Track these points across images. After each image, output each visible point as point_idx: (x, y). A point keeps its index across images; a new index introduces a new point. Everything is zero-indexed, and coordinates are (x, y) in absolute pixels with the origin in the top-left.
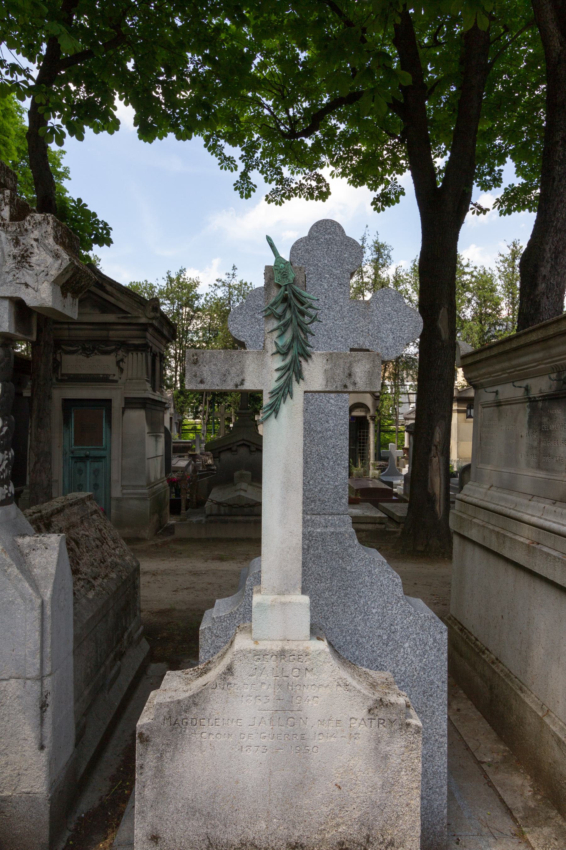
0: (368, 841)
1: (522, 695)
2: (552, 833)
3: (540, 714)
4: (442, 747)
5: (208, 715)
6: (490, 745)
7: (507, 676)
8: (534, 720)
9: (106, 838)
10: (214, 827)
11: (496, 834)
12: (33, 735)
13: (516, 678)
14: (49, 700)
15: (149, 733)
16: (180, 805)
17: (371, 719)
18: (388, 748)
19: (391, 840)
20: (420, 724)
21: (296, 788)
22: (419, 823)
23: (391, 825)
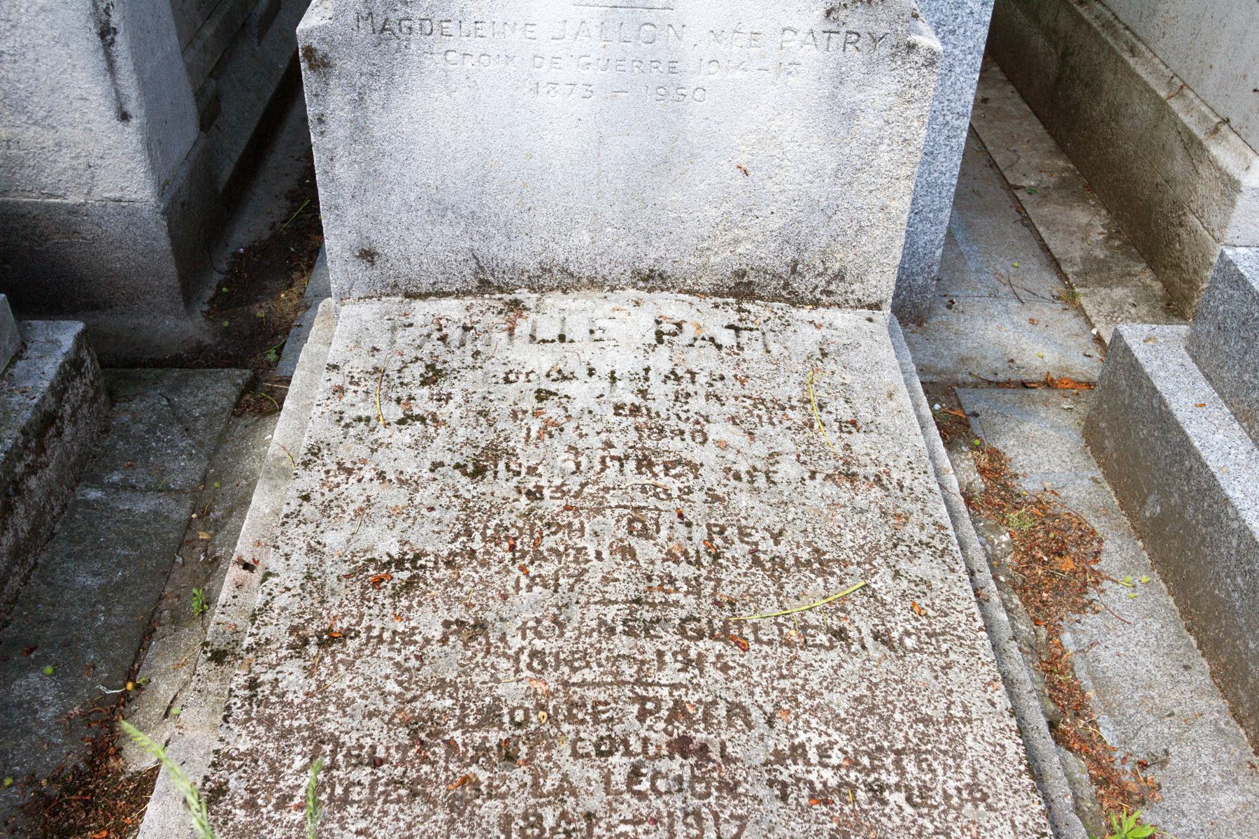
0: (794, 271)
1: (1131, 61)
3: (1163, 94)
4: (954, 137)
5: (458, 13)
6: (1038, 160)
7: (1108, 25)
8: (1145, 107)
9: (290, 286)
10: (486, 238)
12: (99, 90)
13: (1127, 28)
14: (115, 19)
15: (326, 48)
16: (413, 196)
17: (830, 32)
18: (861, 96)
19: (840, 270)
20: (938, 46)
21: (654, 170)
22: (900, 242)
23: (843, 245)
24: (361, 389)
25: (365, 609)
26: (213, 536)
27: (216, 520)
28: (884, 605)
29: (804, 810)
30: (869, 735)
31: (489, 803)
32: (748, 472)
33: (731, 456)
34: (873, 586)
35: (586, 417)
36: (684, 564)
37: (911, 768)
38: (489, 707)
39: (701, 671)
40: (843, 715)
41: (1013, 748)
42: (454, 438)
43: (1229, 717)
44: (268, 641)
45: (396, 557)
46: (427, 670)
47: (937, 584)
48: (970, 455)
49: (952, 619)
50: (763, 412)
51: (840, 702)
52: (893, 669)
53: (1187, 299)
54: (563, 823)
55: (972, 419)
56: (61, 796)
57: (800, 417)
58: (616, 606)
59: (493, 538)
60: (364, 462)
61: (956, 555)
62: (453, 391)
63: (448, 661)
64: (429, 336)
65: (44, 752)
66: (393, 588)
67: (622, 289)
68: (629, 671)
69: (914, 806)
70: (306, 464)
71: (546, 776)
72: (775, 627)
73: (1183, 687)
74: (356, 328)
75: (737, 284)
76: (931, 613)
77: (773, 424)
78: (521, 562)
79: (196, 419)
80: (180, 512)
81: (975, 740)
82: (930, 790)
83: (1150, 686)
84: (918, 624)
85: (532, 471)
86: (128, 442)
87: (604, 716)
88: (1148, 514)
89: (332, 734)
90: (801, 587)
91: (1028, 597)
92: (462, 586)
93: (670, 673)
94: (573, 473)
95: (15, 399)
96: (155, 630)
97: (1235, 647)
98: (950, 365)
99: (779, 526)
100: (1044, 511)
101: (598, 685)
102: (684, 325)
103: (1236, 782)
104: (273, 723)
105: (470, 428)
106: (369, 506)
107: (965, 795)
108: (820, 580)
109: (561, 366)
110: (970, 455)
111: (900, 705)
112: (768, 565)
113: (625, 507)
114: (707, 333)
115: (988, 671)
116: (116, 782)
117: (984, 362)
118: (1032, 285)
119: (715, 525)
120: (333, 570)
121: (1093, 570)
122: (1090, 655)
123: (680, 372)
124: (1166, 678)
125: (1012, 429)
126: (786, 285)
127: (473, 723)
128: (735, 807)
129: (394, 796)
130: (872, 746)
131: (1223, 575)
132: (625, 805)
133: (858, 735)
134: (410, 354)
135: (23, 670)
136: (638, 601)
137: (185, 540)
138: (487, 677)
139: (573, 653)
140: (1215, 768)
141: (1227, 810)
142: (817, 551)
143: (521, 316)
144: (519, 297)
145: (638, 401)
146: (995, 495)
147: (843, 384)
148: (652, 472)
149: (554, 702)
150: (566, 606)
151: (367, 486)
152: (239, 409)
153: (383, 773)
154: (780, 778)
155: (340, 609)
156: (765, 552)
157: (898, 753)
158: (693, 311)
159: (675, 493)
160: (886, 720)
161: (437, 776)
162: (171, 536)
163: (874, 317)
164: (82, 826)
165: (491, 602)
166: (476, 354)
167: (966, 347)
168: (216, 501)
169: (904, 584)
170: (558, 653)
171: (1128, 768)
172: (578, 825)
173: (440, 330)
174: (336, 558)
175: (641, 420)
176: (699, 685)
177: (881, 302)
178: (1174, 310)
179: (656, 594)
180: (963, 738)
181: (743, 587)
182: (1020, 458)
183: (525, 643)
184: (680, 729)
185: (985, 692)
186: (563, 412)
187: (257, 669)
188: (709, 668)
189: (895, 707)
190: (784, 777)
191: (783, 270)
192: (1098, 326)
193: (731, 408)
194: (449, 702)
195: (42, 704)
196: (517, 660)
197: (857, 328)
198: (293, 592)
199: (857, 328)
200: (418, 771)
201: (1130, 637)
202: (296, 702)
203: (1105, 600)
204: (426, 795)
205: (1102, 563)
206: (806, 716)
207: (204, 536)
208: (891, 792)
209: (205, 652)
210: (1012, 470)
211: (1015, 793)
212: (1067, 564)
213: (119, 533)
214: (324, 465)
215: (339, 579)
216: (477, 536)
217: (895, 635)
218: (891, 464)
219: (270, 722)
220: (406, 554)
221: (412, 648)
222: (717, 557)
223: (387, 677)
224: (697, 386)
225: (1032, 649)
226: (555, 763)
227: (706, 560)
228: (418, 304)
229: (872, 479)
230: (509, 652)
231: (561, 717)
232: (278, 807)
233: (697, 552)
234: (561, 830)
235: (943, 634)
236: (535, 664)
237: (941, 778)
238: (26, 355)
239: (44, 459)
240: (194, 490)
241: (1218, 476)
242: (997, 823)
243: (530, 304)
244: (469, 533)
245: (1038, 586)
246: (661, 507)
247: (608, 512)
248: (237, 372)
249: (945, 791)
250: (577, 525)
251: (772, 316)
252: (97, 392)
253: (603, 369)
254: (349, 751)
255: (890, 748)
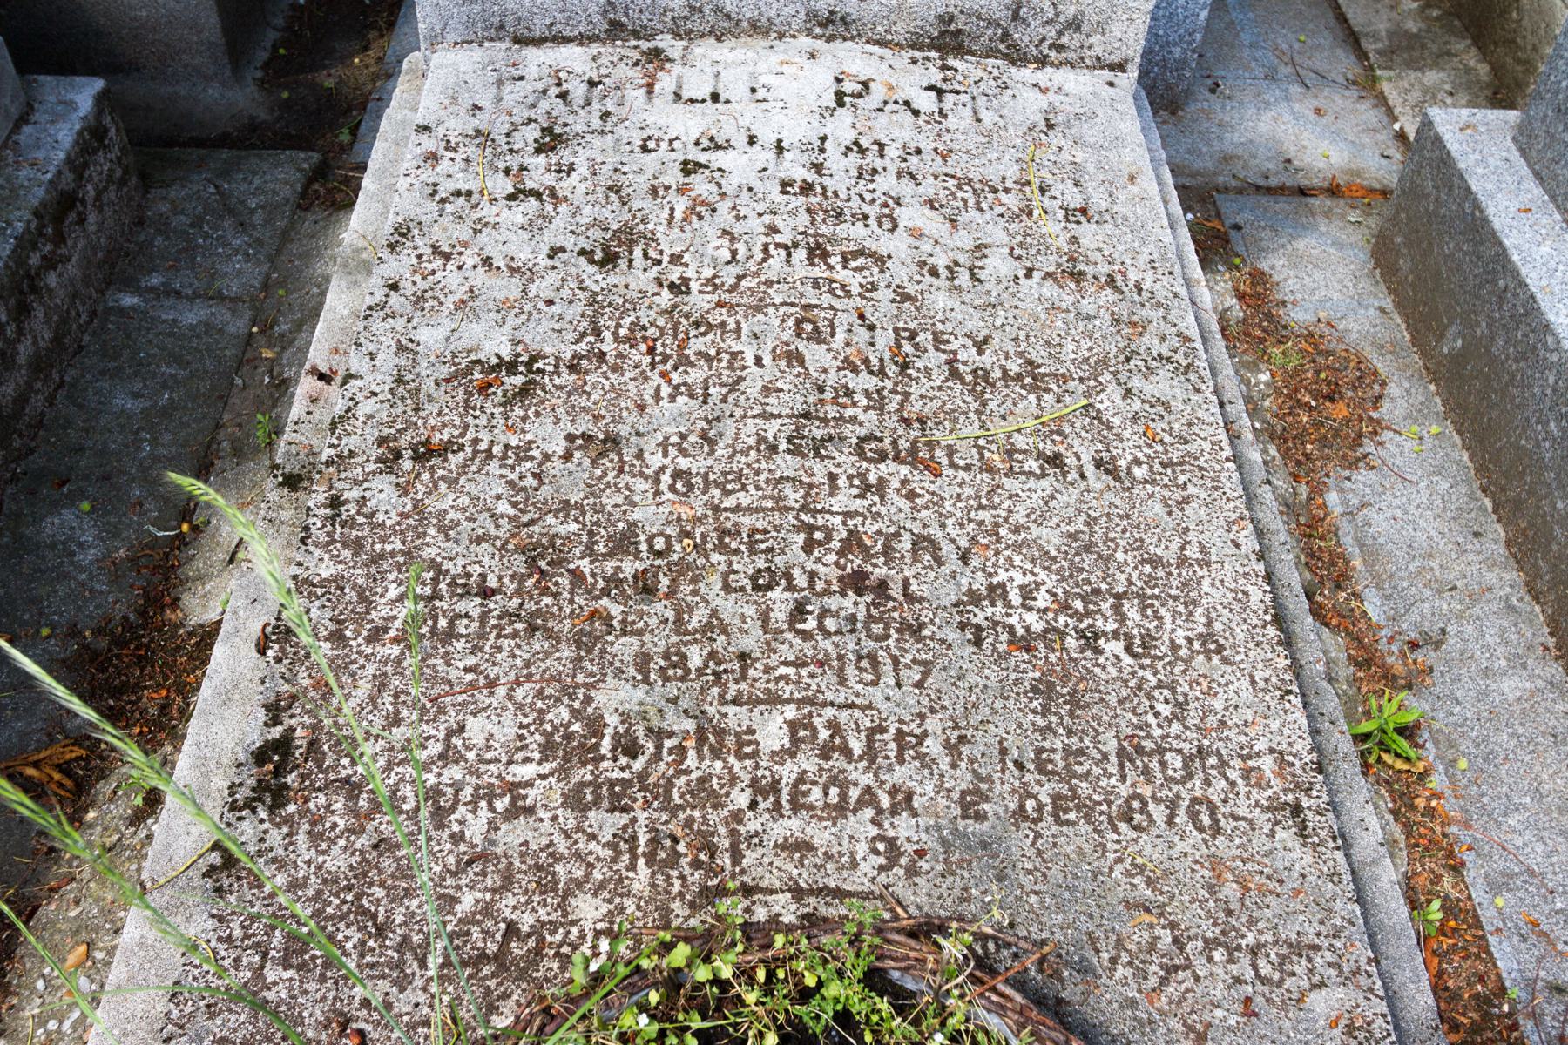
0: (1016, 16)
2: (1443, 82)
9: (366, 48)
11: (1310, 79)
19: (1075, 17)
24: (459, 157)
25: (469, 419)
26: (279, 354)
27: (283, 335)
28: (1110, 428)
29: (1002, 657)
30: (1084, 575)
31: (622, 640)
32: (948, 267)
33: (926, 247)
34: (1098, 405)
35: (745, 195)
36: (864, 374)
37: (1133, 613)
38: (623, 534)
39: (882, 498)
40: (1053, 553)
41: (1258, 595)
42: (578, 218)
43: (1523, 593)
44: (352, 454)
45: (507, 359)
46: (547, 490)
47: (1177, 405)
48: (1227, 276)
49: (1193, 448)
50: (969, 195)
51: (1050, 537)
52: (1118, 502)
53: (1520, 86)
54: (712, 664)
55: (1233, 233)
56: (110, 650)
57: (1016, 202)
58: (780, 421)
59: (627, 339)
60: (466, 245)
61: (1203, 373)
62: (576, 160)
63: (573, 479)
64: (545, 92)
65: (87, 600)
66: (504, 395)
67: (793, 36)
68: (793, 496)
69: (1135, 656)
70: (392, 247)
71: (691, 612)
72: (974, 451)
73: (1471, 557)
74: (451, 81)
75: (942, 33)
76: (1167, 439)
77: (981, 210)
78: (662, 367)
79: (253, 212)
80: (238, 325)
81: (1213, 585)
82: (1154, 639)
83: (1430, 555)
84: (1150, 452)
85: (676, 259)
86: (168, 238)
87: (762, 546)
88: (1445, 350)
89: (433, 561)
90: (1009, 404)
91: (1288, 449)
92: (589, 394)
93: (844, 499)
94: (728, 263)
95: (23, 173)
96: (212, 464)
97: (1539, 507)
98: (1209, 165)
99: (984, 333)
100: (1316, 346)
101: (756, 510)
102: (872, 85)
103: (1524, 666)
104: (361, 546)
105: (598, 207)
106: (472, 299)
107: (1196, 645)
108: (1032, 398)
109: (714, 132)
110: (1227, 276)
111: (1123, 543)
112: (969, 378)
113: (793, 305)
114: (901, 96)
115: (1232, 509)
116: (174, 636)
117: (1253, 162)
118: (1320, 63)
119: (905, 329)
120: (429, 374)
121: (1371, 418)
122: (1359, 518)
123: (865, 143)
124: (1450, 546)
125: (1283, 246)
126: (1006, 36)
127: (604, 551)
128: (918, 651)
129: (509, 630)
130: (1087, 588)
131: (1533, 420)
132: (787, 646)
133: (1071, 576)
134: (521, 114)
135: (55, 506)
136: (806, 415)
137: (245, 358)
138: (620, 500)
139: (725, 474)
140: (1501, 650)
141: (1511, 697)
142: (1030, 363)
143: (662, 69)
144: (661, 45)
145: (811, 177)
146: (1257, 324)
147: (1072, 163)
148: (826, 263)
149: (702, 529)
150: (718, 419)
151: (470, 274)
152: (305, 201)
153: (496, 604)
154: (974, 621)
155: (439, 417)
156: (965, 363)
157: (1118, 596)
158: (884, 67)
159: (855, 290)
160: (1105, 560)
161: (560, 609)
162: (228, 352)
163: (1116, 81)
164: (137, 685)
165: (625, 414)
166: (605, 115)
167: (1233, 139)
168: (282, 310)
169: (1137, 405)
170: (707, 474)
171: (1395, 648)
172: (730, 666)
173: (559, 85)
174: (433, 359)
175: (814, 200)
176: (878, 514)
177: (1126, 61)
178: (1502, 100)
179: (828, 407)
180: (1199, 583)
181: (937, 403)
182: (1290, 282)
183: (667, 461)
184: (854, 562)
185: (1229, 531)
186: (715, 189)
187: (340, 485)
188: (891, 495)
189: (1117, 545)
190: (979, 619)
191: (1002, 15)
192: (1402, 119)
193: (928, 188)
194: (574, 527)
195: (81, 545)
196: (657, 481)
197: (1094, 94)
198: (380, 397)
199: (1094, 94)
200: (537, 603)
201: (1412, 500)
202: (388, 523)
203: (1383, 453)
204: (546, 629)
205: (1383, 410)
206: (1008, 553)
207: (268, 354)
208: (1107, 640)
209: (275, 476)
210: (1279, 297)
211: (1257, 645)
212: (1340, 411)
213: (163, 349)
214: (415, 248)
215: (437, 383)
216: (607, 335)
217: (1122, 463)
218: (1128, 262)
219: (357, 546)
220: (519, 355)
221: (528, 465)
222: (905, 366)
223: (498, 497)
224: (887, 161)
225: (1289, 508)
226: (702, 598)
227: (892, 370)
228: (531, 52)
229: (1103, 280)
230: (647, 471)
231: (710, 546)
232: (370, 640)
233: (881, 360)
234: (709, 671)
235: (1181, 464)
236: (679, 486)
237: (1169, 626)
238: (33, 118)
239: (63, 251)
240: (253, 299)
241: (1539, 297)
242: (1232, 678)
243: (672, 54)
244: (597, 332)
245: (1301, 437)
246: (837, 306)
247: (771, 310)
248: (302, 155)
249: (1172, 641)
250: (731, 325)
251: (985, 76)
252: (126, 171)
253: (767, 137)
254: (454, 579)
255: (1109, 591)
